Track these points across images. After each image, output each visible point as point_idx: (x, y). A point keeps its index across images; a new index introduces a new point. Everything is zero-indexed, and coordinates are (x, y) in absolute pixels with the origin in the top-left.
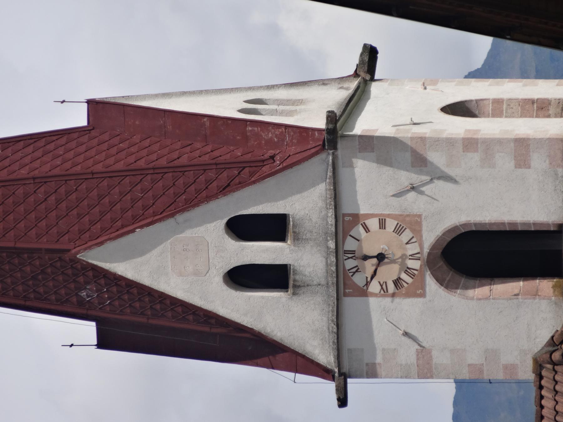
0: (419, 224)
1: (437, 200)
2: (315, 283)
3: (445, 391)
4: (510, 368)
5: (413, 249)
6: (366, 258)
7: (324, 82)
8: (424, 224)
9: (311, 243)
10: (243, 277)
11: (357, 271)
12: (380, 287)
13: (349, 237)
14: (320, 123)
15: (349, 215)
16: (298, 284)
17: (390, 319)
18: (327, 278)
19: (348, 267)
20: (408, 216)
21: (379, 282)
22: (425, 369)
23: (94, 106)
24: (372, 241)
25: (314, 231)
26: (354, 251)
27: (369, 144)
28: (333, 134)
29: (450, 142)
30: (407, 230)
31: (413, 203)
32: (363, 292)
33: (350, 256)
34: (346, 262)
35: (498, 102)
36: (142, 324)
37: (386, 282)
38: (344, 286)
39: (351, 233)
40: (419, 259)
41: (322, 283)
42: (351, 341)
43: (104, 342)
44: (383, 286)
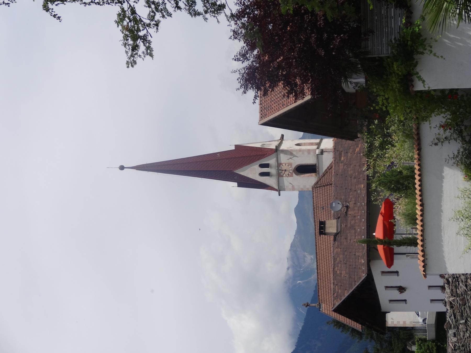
3: (296, 193)
4: (308, 188)
5: (291, 169)
7: (275, 141)
10: (262, 174)
14: (274, 148)
17: (287, 181)
22: (293, 189)
23: (236, 146)
24: (284, 167)
27: (283, 151)
28: (277, 150)
29: (296, 150)
31: (291, 161)
32: (282, 176)
35: (304, 143)
36: (245, 183)
38: (279, 176)
42: (281, 185)
43: (239, 186)
44: (286, 175)
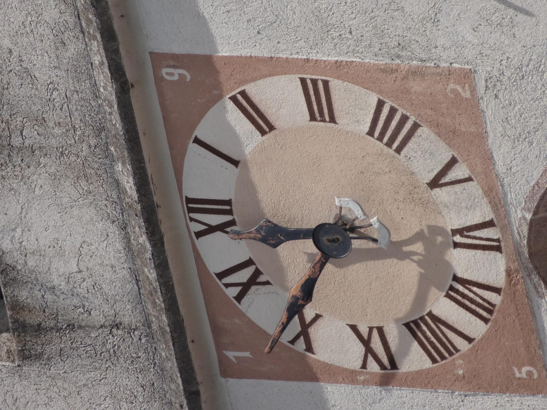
0: (472, 108)
1: (528, 13)
2: (97, 318)
5: (461, 207)
6: (275, 235)
8: (490, 109)
9: (50, 164)
11: (253, 281)
12: (360, 349)
13: (193, 148)
15: (178, 60)
16: (32, 320)
18: (139, 300)
19: (215, 265)
20: (416, 73)
21: (354, 328)
25: (52, 118)
26: (228, 202)
30: (424, 131)
33: (215, 220)
34: (203, 243)
37: (380, 330)
39: (200, 132)
40: (498, 249)
41: (126, 321)
